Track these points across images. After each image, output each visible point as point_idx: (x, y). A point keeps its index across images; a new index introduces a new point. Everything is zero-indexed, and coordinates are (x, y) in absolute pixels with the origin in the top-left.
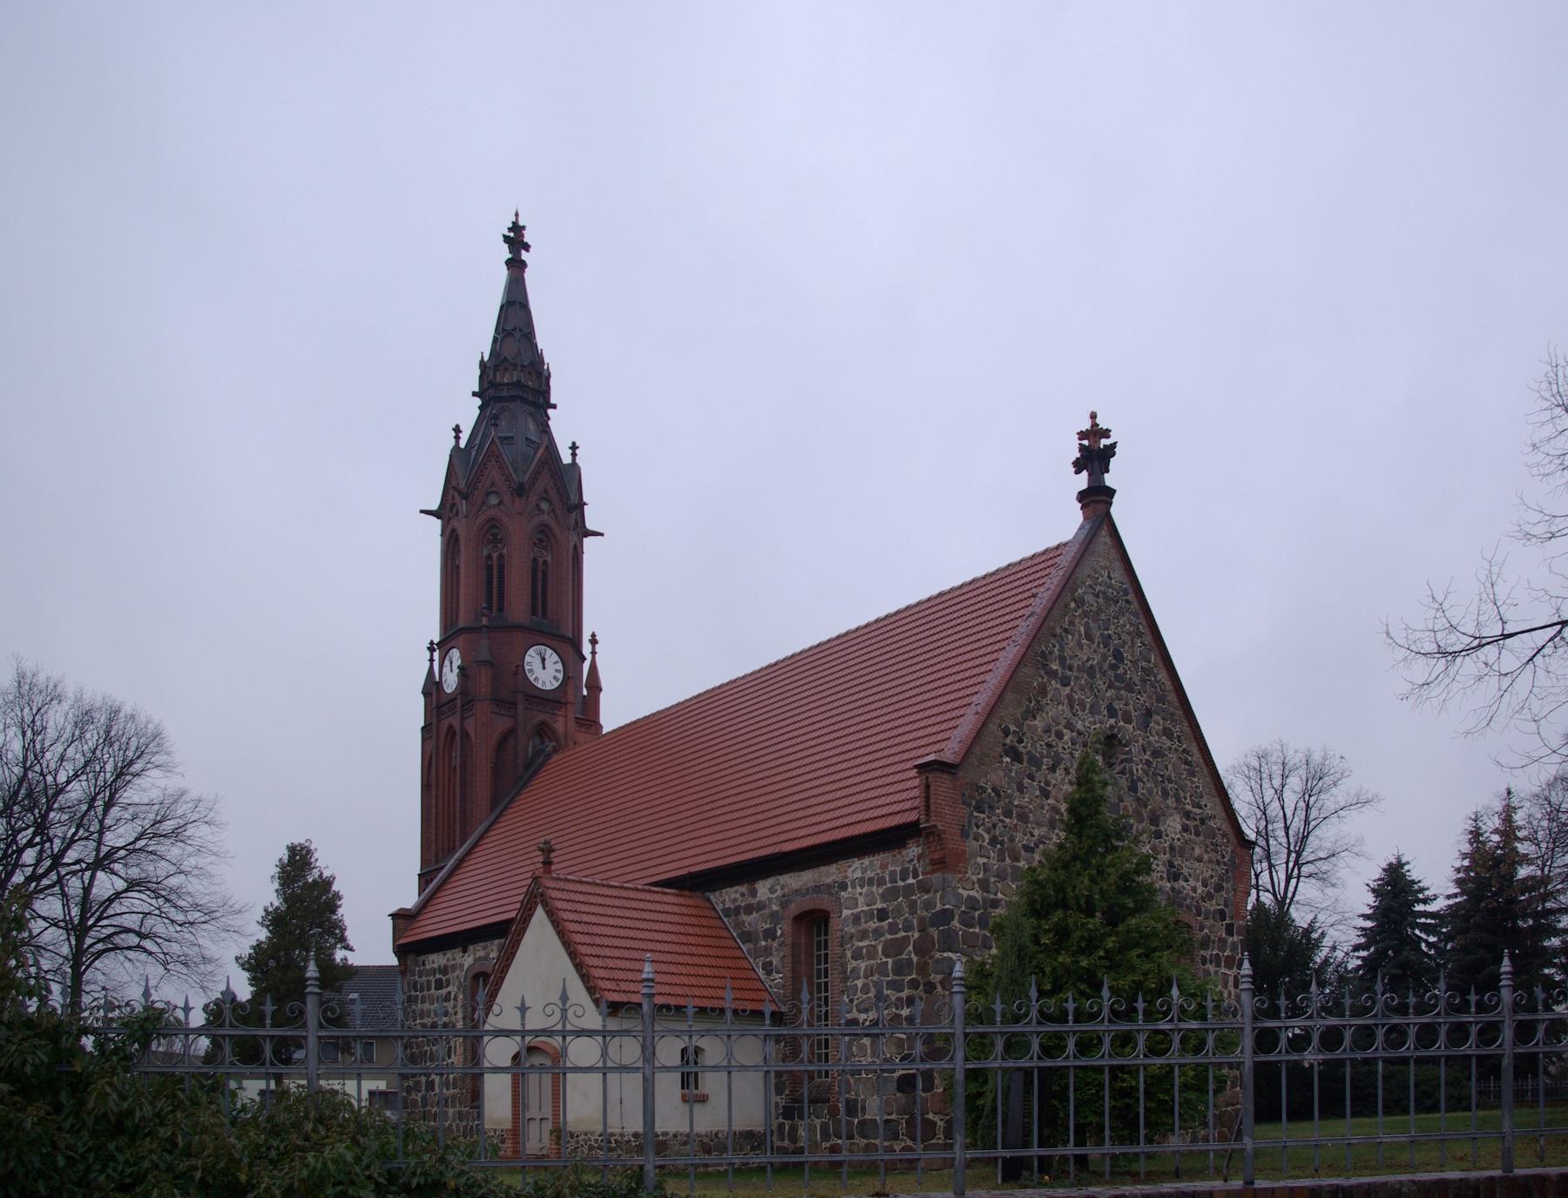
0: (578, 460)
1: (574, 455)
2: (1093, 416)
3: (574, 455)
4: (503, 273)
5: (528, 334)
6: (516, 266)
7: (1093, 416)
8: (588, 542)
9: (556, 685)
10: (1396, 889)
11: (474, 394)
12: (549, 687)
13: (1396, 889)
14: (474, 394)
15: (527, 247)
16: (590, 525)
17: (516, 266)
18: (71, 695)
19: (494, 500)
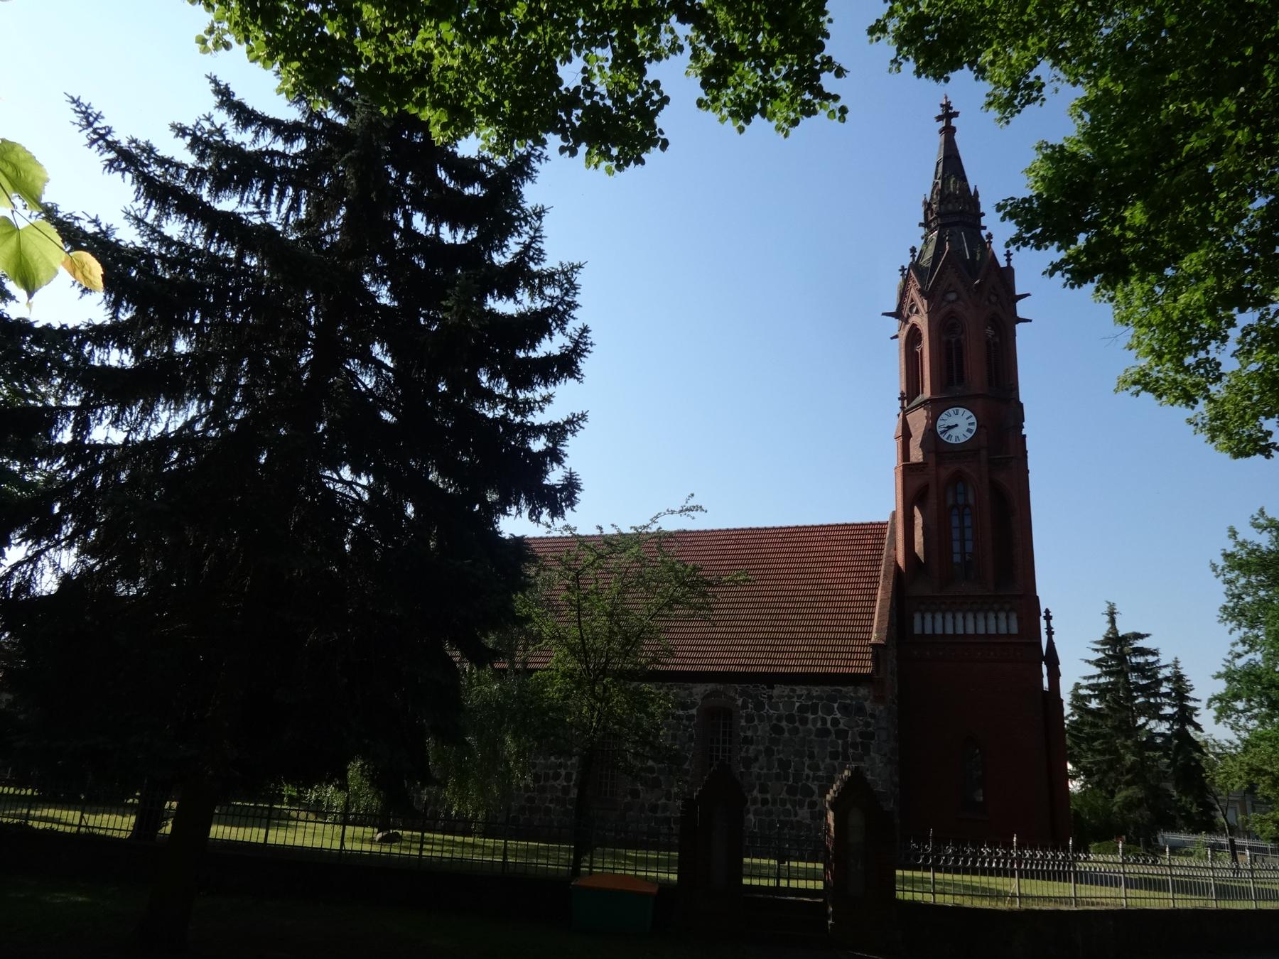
0: (1012, 264)
1: (1009, 260)
2: (1116, 391)
3: (1009, 260)
4: (939, 140)
5: (962, 177)
6: (949, 132)
7: (1116, 391)
8: (1019, 327)
9: (970, 436)
10: (1059, 249)
11: (921, 225)
12: (963, 440)
13: (1059, 249)
14: (921, 225)
15: (956, 114)
16: (1020, 314)
17: (949, 132)
18: (1144, 362)
19: (952, 297)
